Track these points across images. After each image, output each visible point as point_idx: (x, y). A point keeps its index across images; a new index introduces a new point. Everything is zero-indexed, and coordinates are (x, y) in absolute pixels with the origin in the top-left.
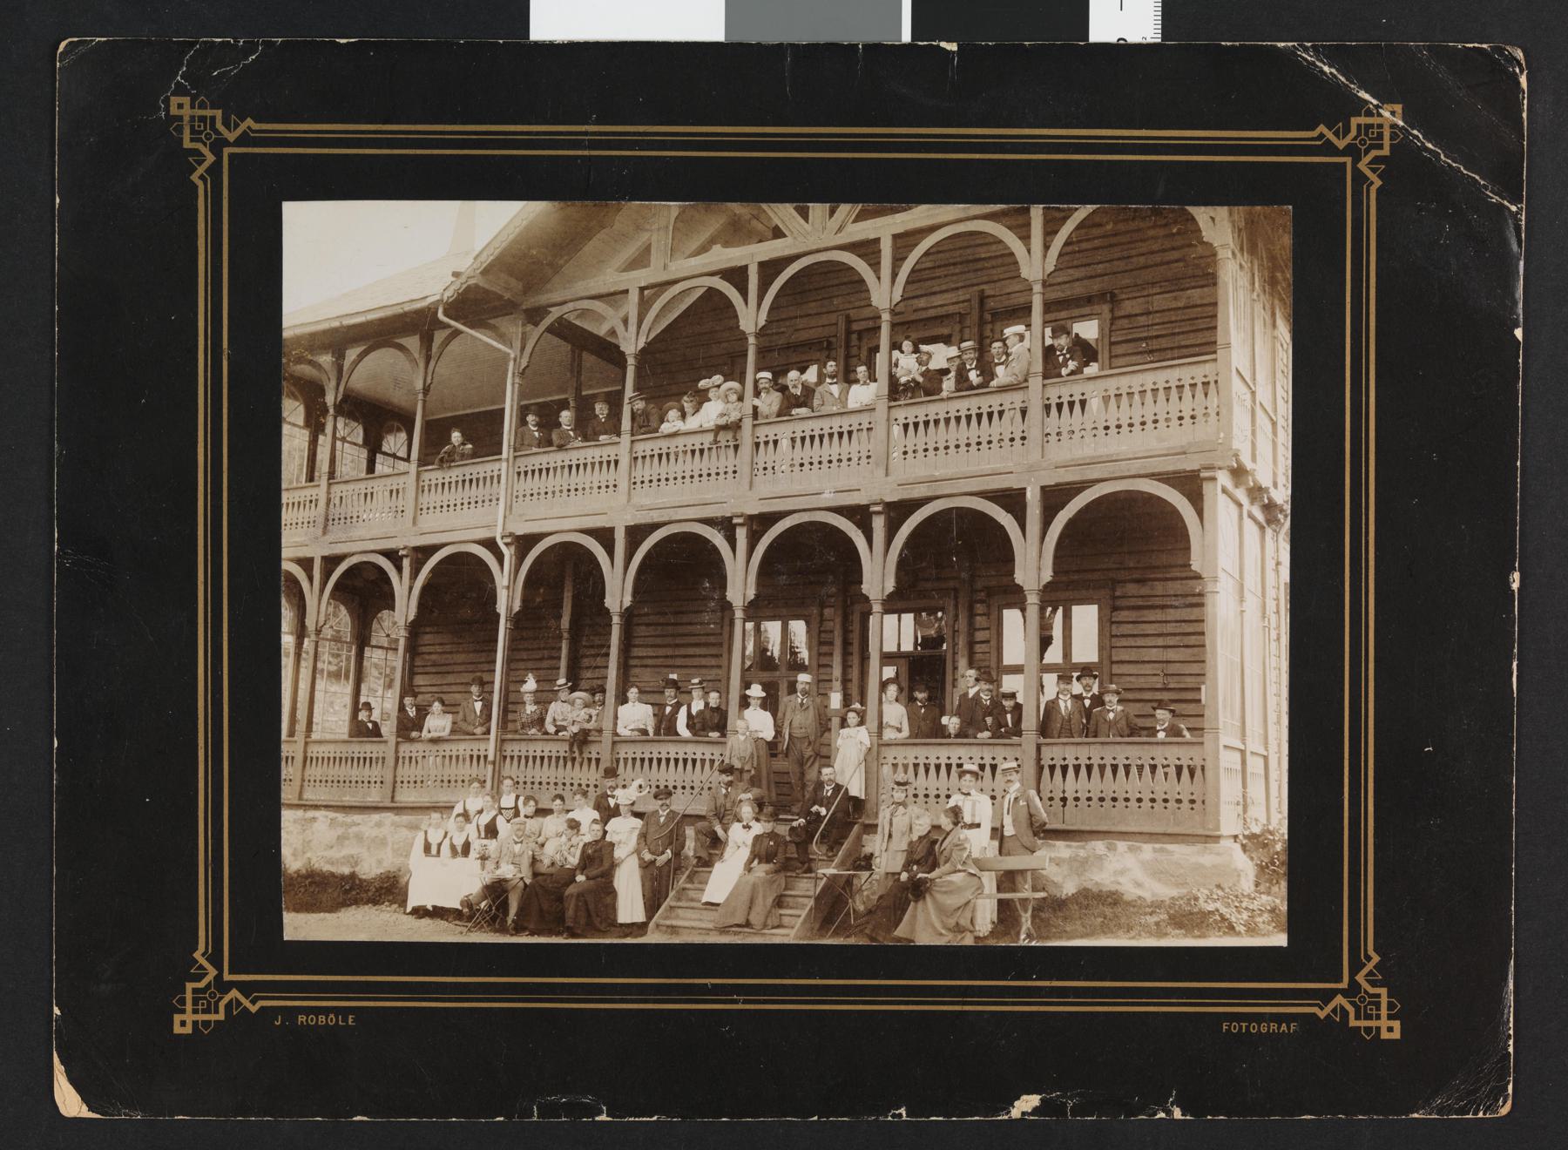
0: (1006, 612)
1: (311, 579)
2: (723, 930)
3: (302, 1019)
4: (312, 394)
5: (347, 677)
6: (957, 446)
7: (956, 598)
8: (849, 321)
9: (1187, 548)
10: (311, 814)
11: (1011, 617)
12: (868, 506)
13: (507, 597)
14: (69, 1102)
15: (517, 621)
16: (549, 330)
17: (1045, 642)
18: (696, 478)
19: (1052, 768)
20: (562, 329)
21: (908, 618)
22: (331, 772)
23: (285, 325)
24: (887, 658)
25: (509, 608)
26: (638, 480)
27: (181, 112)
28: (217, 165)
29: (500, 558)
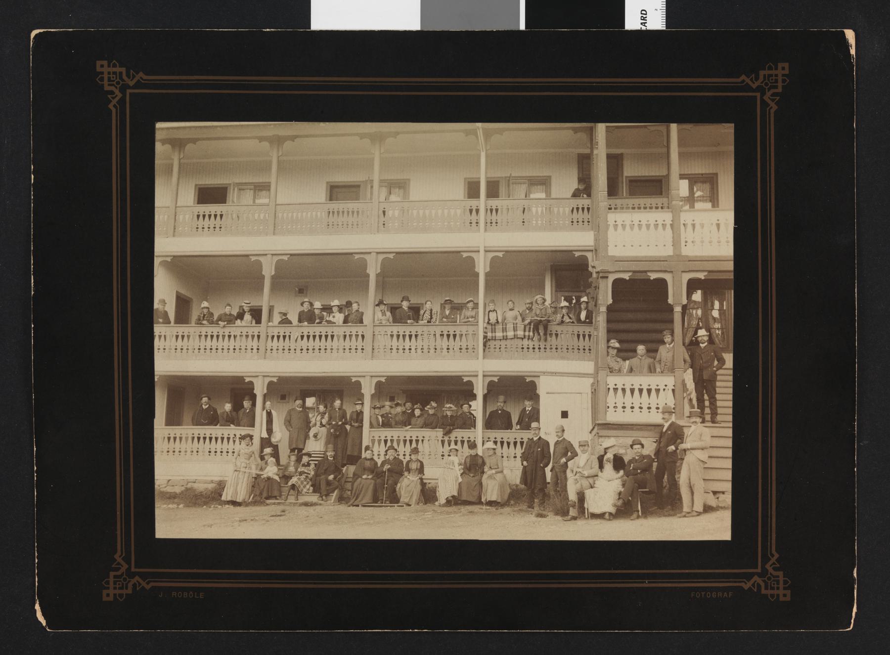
3: (174, 594)
14: (850, 35)
27: (102, 70)
28: (751, 89)
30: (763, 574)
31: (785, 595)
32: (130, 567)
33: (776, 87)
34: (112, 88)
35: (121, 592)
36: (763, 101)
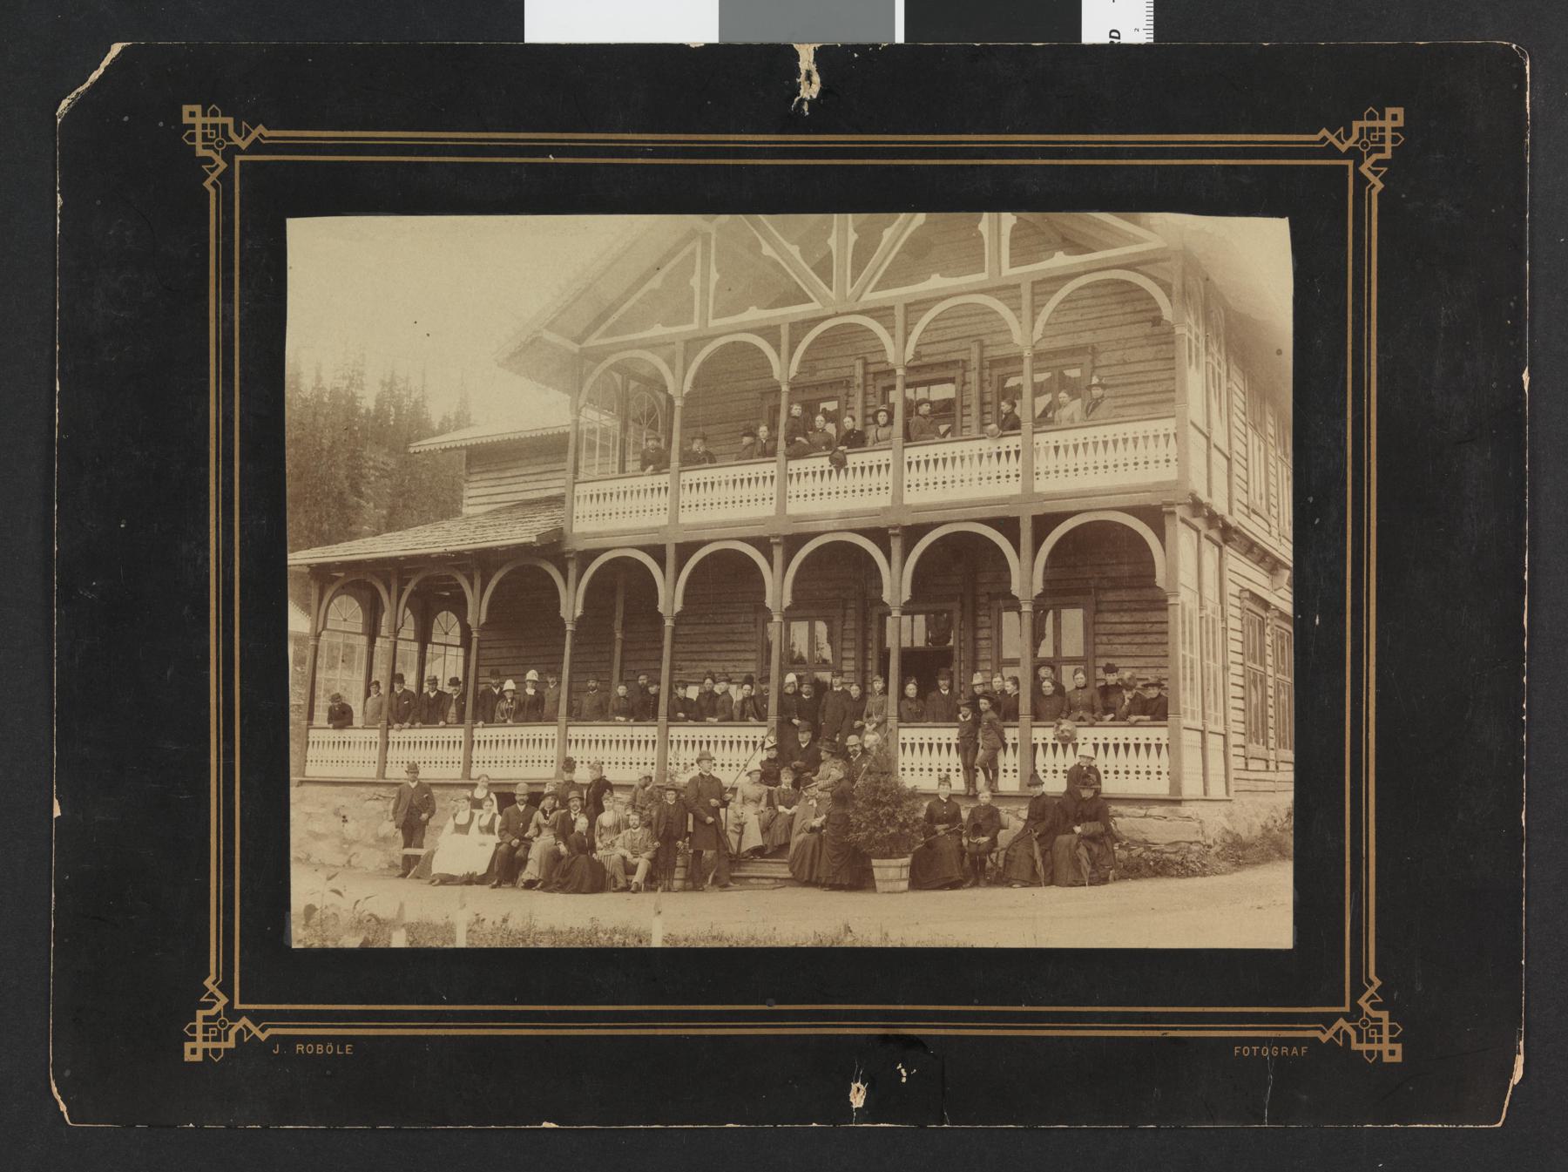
0: (1005, 615)
8: (866, 364)
11: (1009, 618)
12: (886, 530)
21: (920, 619)
30: (231, 1013)
31: (1392, 1053)
32: (1356, 166)
35: (1386, 1031)
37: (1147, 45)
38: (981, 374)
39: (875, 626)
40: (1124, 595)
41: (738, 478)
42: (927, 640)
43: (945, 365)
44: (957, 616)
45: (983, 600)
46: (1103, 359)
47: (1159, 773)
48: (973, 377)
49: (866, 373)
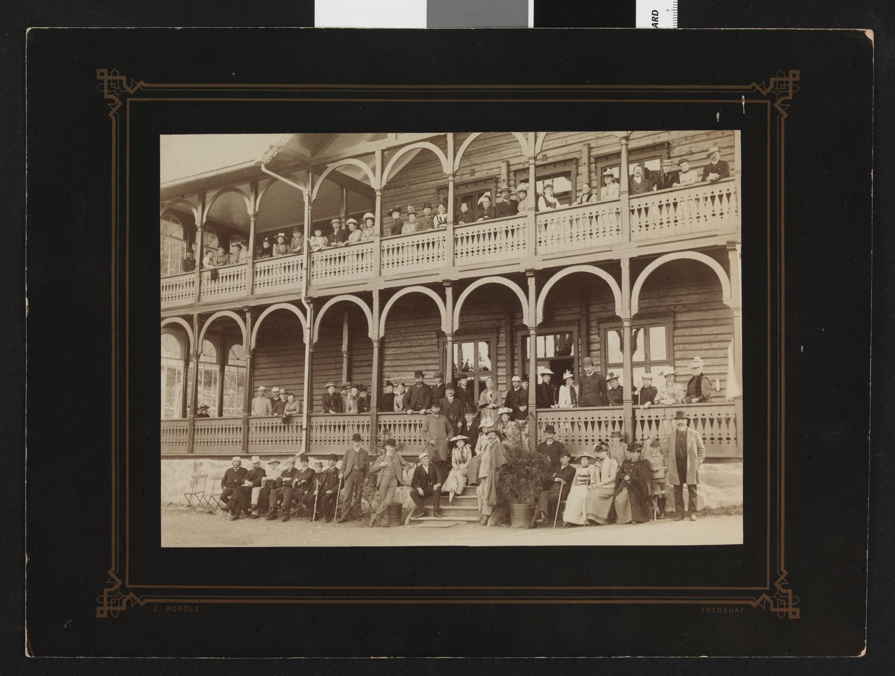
1: (192, 328)
2: (421, 521)
4: (187, 222)
5: (215, 383)
6: (484, 250)
7: (579, 325)
8: (509, 165)
9: (721, 291)
10: (198, 461)
12: (525, 273)
13: (309, 333)
15: (316, 347)
16: (328, 177)
17: (634, 348)
18: (396, 264)
19: (642, 422)
20: (335, 176)
21: (550, 339)
22: (266, 436)
23: (161, 182)
24: (538, 361)
25: (311, 340)
26: (459, 252)
27: (102, 78)
28: (135, 591)
29: (304, 312)
31: (102, 74)
32: (772, 104)
33: (109, 593)
34: (112, 97)
36: (773, 108)
37: (674, 30)
38: (589, 167)
39: (519, 343)
40: (695, 316)
41: (421, 242)
42: (556, 353)
43: (564, 162)
44: (575, 336)
45: (594, 324)
46: (676, 152)
47: (728, 439)
48: (583, 170)
49: (509, 172)
